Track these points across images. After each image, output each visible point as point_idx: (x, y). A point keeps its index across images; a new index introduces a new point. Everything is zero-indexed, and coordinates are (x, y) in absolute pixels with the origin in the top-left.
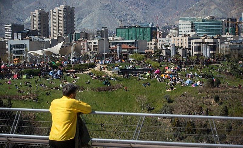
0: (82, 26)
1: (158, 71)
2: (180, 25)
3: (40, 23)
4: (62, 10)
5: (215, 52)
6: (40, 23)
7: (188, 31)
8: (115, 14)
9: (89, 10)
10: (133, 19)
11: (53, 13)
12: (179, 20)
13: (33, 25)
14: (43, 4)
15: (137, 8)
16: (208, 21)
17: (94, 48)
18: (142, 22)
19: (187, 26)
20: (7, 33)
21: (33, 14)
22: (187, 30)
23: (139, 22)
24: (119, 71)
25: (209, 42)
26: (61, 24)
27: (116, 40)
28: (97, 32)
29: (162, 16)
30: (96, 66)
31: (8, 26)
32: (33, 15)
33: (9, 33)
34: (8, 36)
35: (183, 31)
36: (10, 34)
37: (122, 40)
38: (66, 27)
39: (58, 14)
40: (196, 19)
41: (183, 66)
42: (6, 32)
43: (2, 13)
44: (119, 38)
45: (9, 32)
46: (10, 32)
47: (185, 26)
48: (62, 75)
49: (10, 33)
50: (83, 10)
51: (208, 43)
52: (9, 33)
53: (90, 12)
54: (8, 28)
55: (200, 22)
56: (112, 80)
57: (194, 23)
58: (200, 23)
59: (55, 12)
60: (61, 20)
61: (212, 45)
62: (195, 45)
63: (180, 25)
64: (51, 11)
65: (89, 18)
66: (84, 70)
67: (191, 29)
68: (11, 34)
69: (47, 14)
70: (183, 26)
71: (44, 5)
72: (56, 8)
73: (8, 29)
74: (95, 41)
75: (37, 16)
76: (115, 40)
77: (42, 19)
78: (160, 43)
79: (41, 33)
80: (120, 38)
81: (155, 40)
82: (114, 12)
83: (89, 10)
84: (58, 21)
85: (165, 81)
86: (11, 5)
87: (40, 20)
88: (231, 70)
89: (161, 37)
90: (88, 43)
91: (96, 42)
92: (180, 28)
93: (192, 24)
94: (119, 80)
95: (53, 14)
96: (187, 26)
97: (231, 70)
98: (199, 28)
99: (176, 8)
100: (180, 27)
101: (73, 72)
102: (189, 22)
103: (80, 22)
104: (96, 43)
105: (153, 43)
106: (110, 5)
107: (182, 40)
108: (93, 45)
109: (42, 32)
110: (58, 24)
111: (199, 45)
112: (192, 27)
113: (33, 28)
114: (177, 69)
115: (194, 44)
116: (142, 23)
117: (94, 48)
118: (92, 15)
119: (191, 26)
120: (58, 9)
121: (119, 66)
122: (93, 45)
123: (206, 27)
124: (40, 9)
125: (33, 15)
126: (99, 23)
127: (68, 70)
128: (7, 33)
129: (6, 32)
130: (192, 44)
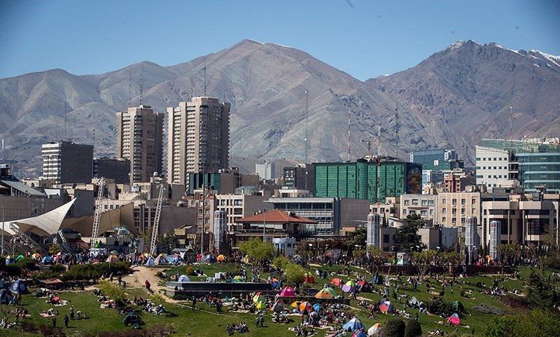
0: (279, 152)
1: (289, 290)
2: (480, 159)
3: (141, 143)
4: (197, 109)
5: (545, 237)
6: (139, 142)
7: (495, 177)
8: (369, 122)
9: (302, 110)
10: (416, 137)
11: (174, 116)
12: (477, 147)
13: (122, 147)
14: (181, 91)
15: (428, 107)
16: (553, 150)
17: (233, 216)
18: (440, 146)
19: (498, 164)
20: (48, 167)
21: (122, 118)
22: (497, 172)
23: (433, 145)
24: (178, 288)
25: (528, 210)
26: (192, 147)
27: (285, 195)
28: (285, 170)
29: (493, 132)
30: (132, 272)
31: (52, 148)
32: (123, 121)
33: (52, 167)
34: (50, 173)
35: (486, 177)
36: (54, 169)
37: (303, 197)
38: (205, 155)
39: (187, 119)
40: (521, 145)
41: (388, 279)
42: (46, 162)
43: (72, 110)
44: (294, 192)
45: (53, 162)
46: (54, 164)
47: (492, 164)
48: (26, 292)
49: (56, 166)
50: (284, 110)
51: (527, 212)
52: (52, 167)
53: (304, 116)
54: (51, 153)
55: (533, 152)
56: (152, 311)
57: (517, 155)
58: (535, 154)
59: (179, 114)
60: (192, 136)
61: (538, 217)
62: (492, 216)
63: (480, 159)
64: (170, 110)
65: (300, 131)
66: (91, 281)
67: (507, 172)
68: (57, 169)
69: (161, 119)
70: (487, 164)
71: (184, 94)
72: (182, 104)
73: (50, 155)
74: (237, 197)
75: (132, 122)
76: (283, 197)
77: (145, 132)
78: (406, 207)
79: (141, 168)
80: (296, 191)
81: (393, 199)
82: (365, 117)
83: (302, 110)
84: (187, 138)
85: (293, 321)
86: (99, 92)
87: (138, 133)
88: (531, 291)
89: (458, 190)
90: (217, 202)
91: (238, 200)
92: (479, 168)
93: (513, 158)
94: (171, 313)
95: (174, 120)
96: (498, 164)
97: (531, 291)
98: (531, 168)
99: (532, 112)
100: (478, 164)
101: (58, 286)
102: (503, 151)
103: (278, 140)
104: (240, 203)
105: (388, 207)
106: (356, 97)
107: (463, 201)
108: (229, 207)
109: (144, 166)
110: (186, 146)
111: (502, 217)
112: (513, 167)
113: (122, 154)
114: (364, 286)
115: (488, 212)
116: (439, 148)
117: (233, 216)
118: (308, 123)
119: (507, 163)
120: (187, 107)
121: (198, 272)
122: (229, 207)
123: (550, 168)
124: (142, 106)
125: (123, 121)
126: (325, 147)
127: (45, 279)
128: (48, 167)
129: (46, 162)
130: (485, 214)
